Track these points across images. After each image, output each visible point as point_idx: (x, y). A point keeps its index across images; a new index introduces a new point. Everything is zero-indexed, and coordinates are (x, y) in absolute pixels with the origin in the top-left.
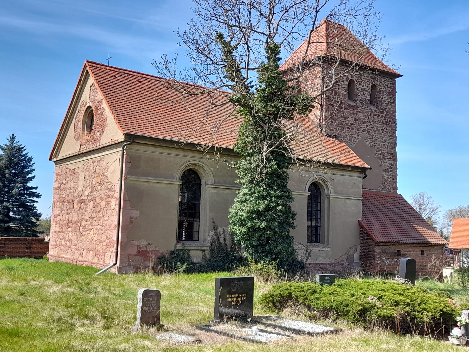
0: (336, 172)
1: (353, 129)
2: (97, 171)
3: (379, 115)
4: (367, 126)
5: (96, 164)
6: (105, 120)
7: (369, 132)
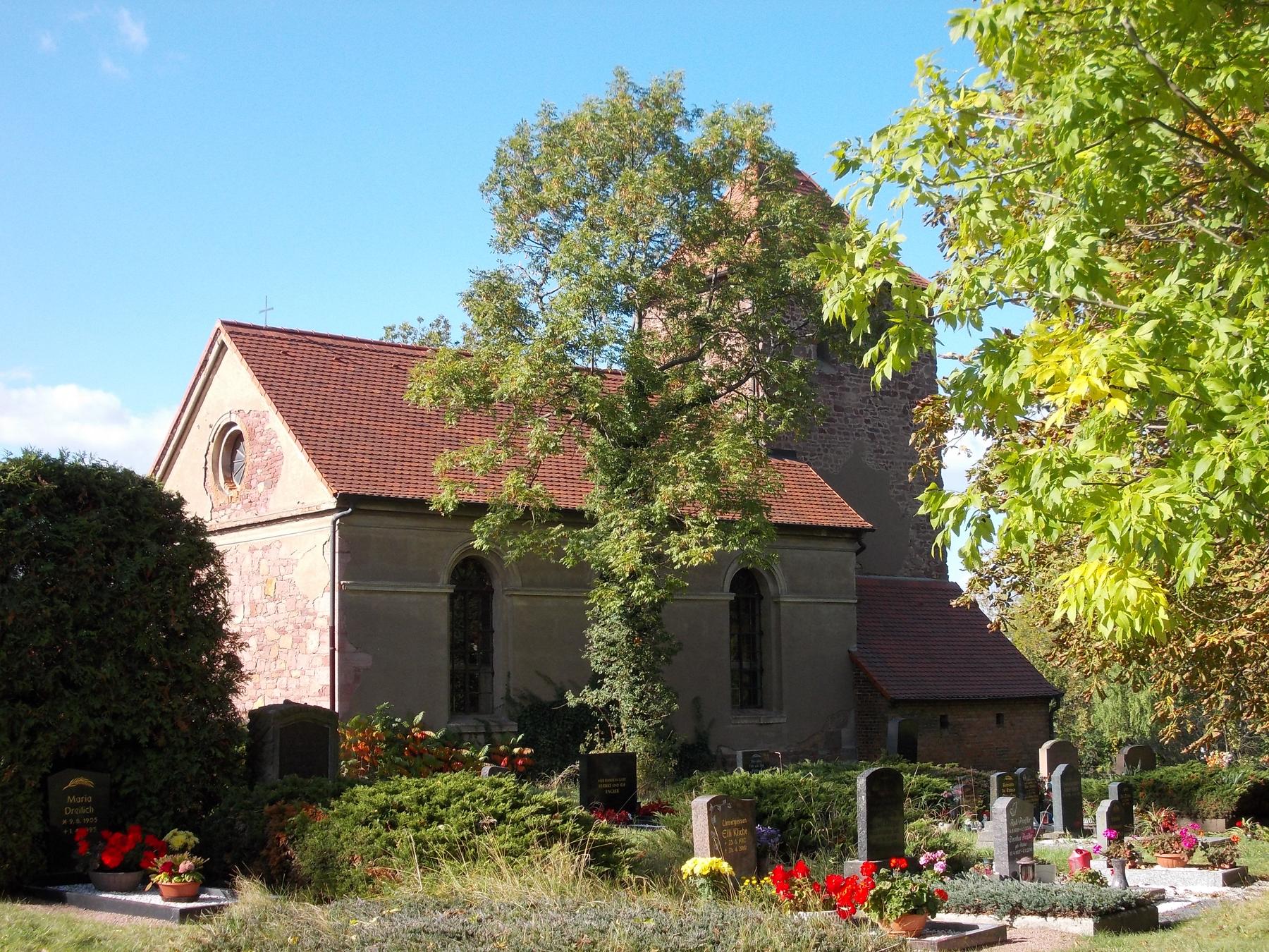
0: (792, 542)
1: (832, 431)
2: (264, 569)
3: (895, 394)
4: (867, 421)
5: (259, 554)
6: (279, 457)
7: (872, 437)
